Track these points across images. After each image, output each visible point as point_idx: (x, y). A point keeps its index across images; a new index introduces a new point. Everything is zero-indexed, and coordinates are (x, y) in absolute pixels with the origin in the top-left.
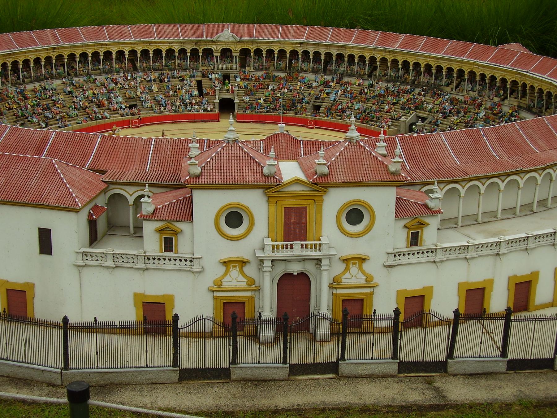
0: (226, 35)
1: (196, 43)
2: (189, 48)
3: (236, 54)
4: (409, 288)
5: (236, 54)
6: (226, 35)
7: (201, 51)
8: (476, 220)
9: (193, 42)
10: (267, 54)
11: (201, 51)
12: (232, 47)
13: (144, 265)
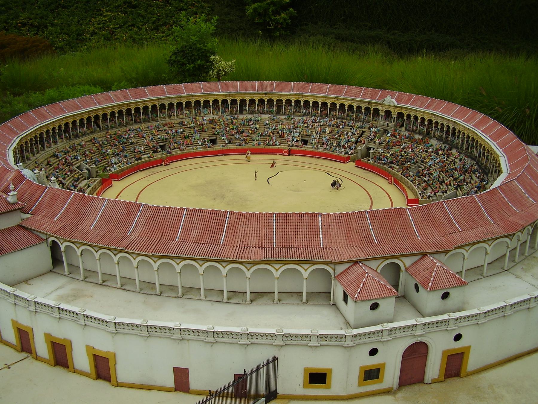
0: (390, 101)
1: (369, 103)
2: (364, 106)
3: (394, 116)
4: (118, 367)
5: (394, 116)
6: (390, 101)
7: (372, 109)
8: (502, 268)
9: (366, 102)
10: (348, 108)
11: (372, 109)
12: (392, 110)
13: (214, 339)
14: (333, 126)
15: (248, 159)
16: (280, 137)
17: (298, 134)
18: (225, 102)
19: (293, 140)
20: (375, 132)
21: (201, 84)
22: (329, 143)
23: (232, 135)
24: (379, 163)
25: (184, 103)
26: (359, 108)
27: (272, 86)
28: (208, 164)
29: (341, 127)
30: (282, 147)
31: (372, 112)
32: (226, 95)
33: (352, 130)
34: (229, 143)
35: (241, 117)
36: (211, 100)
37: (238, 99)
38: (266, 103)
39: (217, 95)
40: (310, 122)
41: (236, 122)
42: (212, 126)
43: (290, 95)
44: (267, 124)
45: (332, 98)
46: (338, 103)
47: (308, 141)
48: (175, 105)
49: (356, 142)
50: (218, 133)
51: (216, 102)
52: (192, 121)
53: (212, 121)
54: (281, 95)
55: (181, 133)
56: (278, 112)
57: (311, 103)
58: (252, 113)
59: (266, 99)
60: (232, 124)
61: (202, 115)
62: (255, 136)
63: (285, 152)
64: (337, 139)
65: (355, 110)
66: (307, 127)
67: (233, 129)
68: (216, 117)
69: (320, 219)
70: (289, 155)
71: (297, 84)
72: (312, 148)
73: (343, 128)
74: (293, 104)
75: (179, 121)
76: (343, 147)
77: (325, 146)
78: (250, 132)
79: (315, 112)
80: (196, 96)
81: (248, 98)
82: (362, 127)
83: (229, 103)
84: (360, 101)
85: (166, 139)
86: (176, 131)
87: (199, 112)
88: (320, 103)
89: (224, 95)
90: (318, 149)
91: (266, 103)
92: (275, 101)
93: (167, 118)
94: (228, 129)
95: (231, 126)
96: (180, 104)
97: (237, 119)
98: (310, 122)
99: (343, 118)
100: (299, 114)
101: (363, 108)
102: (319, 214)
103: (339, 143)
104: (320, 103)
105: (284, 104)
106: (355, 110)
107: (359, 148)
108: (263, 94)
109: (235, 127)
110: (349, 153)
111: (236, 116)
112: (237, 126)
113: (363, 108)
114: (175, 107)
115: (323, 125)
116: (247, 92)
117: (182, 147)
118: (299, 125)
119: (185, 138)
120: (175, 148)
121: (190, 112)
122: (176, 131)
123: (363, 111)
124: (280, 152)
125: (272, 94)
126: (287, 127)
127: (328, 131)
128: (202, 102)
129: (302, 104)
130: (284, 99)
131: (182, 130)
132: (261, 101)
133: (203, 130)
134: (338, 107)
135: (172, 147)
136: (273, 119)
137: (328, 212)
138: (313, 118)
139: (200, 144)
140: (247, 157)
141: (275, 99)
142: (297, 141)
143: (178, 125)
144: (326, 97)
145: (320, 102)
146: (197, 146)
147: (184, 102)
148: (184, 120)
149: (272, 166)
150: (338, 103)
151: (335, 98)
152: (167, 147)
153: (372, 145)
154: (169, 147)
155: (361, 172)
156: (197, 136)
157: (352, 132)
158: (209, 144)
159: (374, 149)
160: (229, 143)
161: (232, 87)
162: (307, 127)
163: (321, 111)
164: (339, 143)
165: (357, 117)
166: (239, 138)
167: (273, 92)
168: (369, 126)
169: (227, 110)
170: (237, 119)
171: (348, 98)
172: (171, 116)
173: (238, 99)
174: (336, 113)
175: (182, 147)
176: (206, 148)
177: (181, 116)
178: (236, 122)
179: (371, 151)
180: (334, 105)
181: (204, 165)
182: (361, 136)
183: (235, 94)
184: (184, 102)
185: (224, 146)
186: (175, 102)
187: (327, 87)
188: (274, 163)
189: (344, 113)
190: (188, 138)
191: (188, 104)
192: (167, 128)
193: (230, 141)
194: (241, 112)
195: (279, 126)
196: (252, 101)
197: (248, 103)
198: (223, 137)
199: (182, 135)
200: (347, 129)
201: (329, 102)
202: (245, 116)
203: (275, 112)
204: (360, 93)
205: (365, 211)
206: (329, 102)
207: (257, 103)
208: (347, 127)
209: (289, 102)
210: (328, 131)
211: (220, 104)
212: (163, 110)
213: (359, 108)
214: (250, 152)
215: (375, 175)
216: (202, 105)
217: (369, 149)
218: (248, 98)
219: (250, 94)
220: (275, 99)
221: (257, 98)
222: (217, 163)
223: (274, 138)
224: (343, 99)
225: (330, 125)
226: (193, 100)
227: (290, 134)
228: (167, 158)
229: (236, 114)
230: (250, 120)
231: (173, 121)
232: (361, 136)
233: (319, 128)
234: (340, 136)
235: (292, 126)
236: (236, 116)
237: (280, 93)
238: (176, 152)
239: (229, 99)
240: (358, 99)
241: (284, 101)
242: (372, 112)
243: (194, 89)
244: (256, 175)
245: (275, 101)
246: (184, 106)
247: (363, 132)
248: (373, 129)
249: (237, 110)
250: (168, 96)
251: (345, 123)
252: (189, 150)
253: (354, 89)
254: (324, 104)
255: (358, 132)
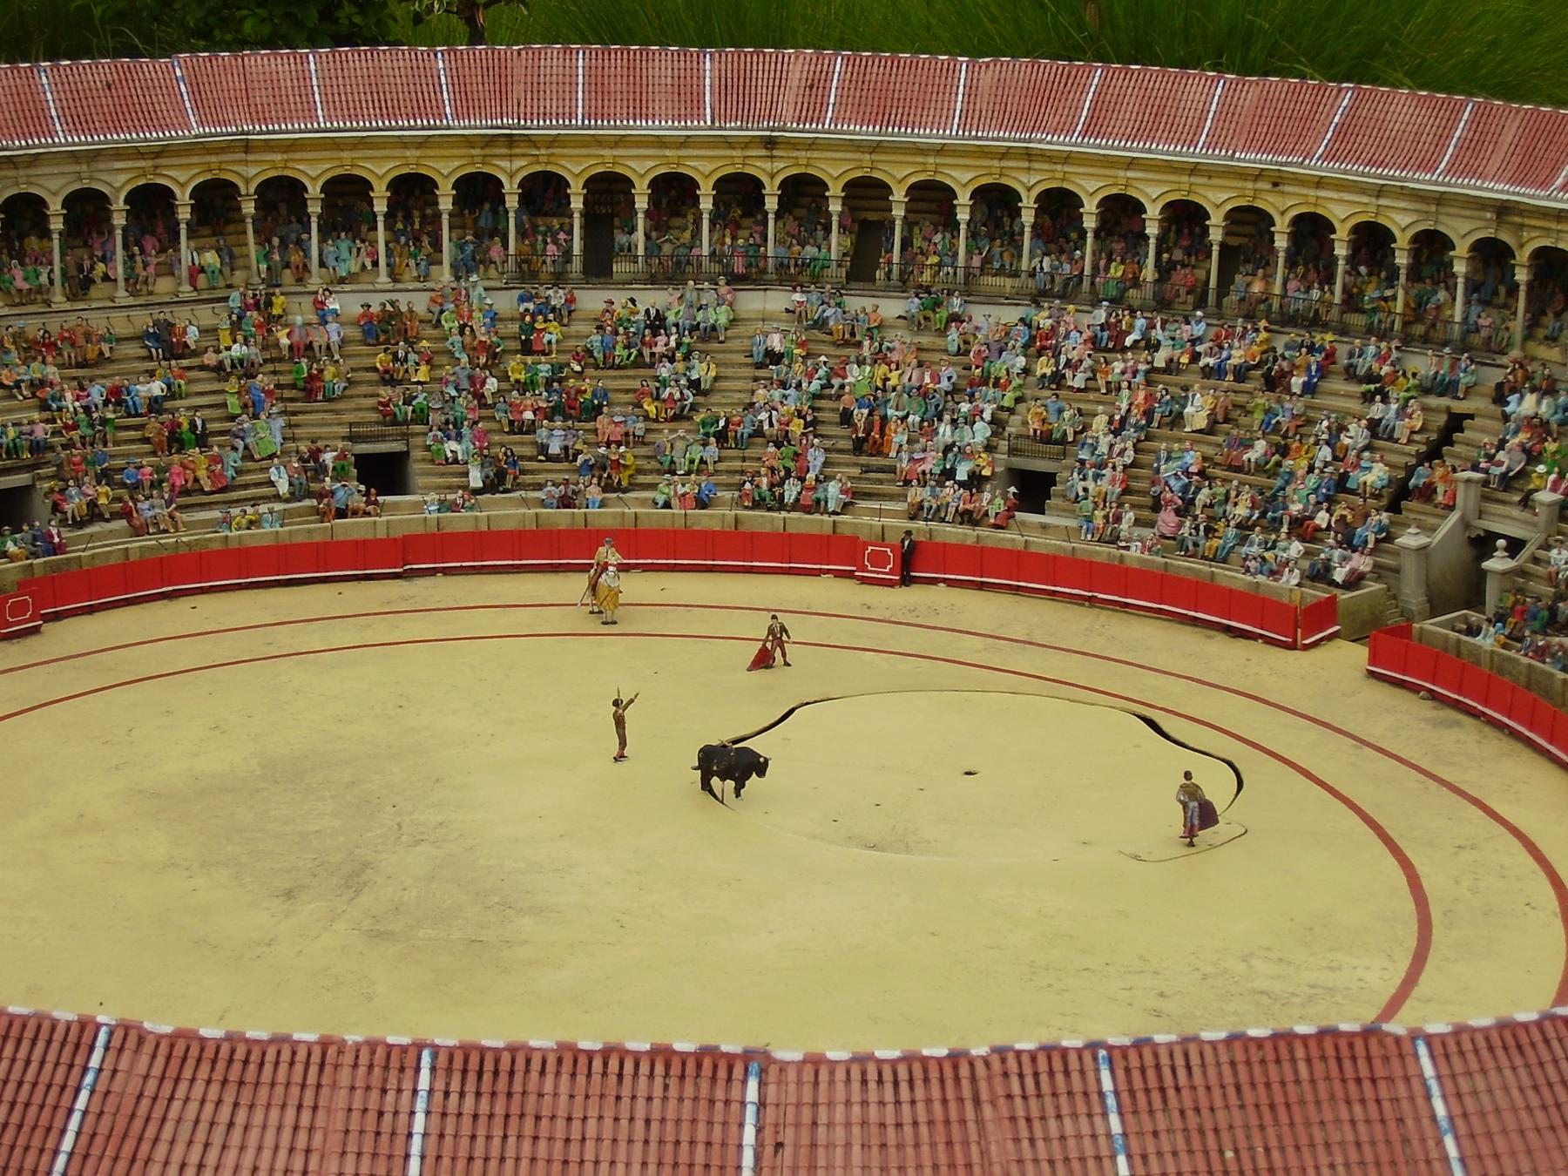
1: (1503, 210)
2: (1463, 233)
7: (1523, 256)
9: (1480, 204)
11: (1523, 256)
14: (1241, 374)
15: (604, 611)
16: (858, 447)
17: (982, 431)
18: (478, 191)
19: (949, 474)
20: (1539, 427)
21: (314, 61)
22: (1203, 496)
23: (518, 428)
24: (1541, 653)
25: (183, 197)
26: (1431, 245)
27: (815, 86)
28: (314, 638)
29: (1297, 382)
30: (866, 520)
31: (1522, 276)
32: (490, 141)
33: (1376, 410)
34: (494, 484)
35: (592, 300)
36: (380, 173)
37: (576, 171)
38: (771, 204)
39: (424, 143)
40: (1075, 347)
41: (553, 333)
42: (381, 360)
43: (941, 151)
44: (774, 357)
45: (1241, 174)
46: (1282, 210)
47: (1049, 479)
48: (119, 205)
49: (1398, 495)
50: (421, 417)
51: (412, 191)
52: (236, 326)
53: (384, 328)
54: (876, 148)
55: (155, 405)
56: (860, 271)
57: (1090, 207)
58: (670, 274)
59: (771, 173)
60: (527, 349)
61: (315, 281)
62: (681, 443)
63: (879, 560)
64: (1260, 468)
65: (1402, 259)
66: (1057, 379)
67: (523, 387)
68: (420, 303)
69: (752, 1093)
70: (907, 581)
71: (991, 71)
72: (1068, 533)
73: (1309, 389)
74: (963, 216)
75: (143, 320)
76: (1301, 528)
77: (1167, 519)
78: (650, 408)
79: (1116, 271)
80: (269, 146)
81: (641, 171)
82: (1445, 387)
83: (512, 202)
84: (1440, 200)
85: (37, 447)
86: (116, 396)
87: (295, 258)
88: (1153, 212)
89: (469, 142)
90: (1114, 539)
91: (771, 204)
92: (835, 190)
93: (58, 297)
94: (492, 384)
95: (515, 367)
96: (151, 203)
97: (564, 315)
98: (1075, 347)
99: (1314, 322)
100: (1008, 283)
101: (1462, 249)
102: (748, 1056)
103: (1269, 502)
104: (1153, 212)
105: (898, 212)
106: (1402, 259)
107: (1410, 539)
108: (747, 143)
109: (544, 370)
110: (1339, 575)
111: (557, 298)
112: (558, 368)
113: (1462, 249)
114: (119, 220)
115: (1171, 367)
116: (642, 128)
117: (147, 509)
118: (998, 368)
119: (175, 441)
120: (94, 513)
121: (231, 259)
122: (116, 396)
123: (1460, 268)
124: (838, 555)
125: (812, 145)
126: (911, 376)
127: (1197, 412)
128: (314, 190)
129: (1028, 217)
130: (899, 178)
131: (157, 388)
132: (740, 193)
133: (310, 388)
134: (1281, 242)
135: (75, 504)
136: (821, 324)
137: (816, 1047)
138: (1101, 315)
139: (283, 488)
140: (594, 587)
141: (835, 174)
142: (975, 481)
143: (133, 349)
144: (1194, 170)
145: (1153, 197)
146: (255, 501)
147: (182, 182)
148: (180, 316)
149: (763, 660)
150: (1282, 210)
151: (1259, 175)
152: (41, 506)
153: (1506, 521)
154: (56, 508)
155: (1402, 718)
156: (269, 432)
157: (1373, 425)
158: (351, 492)
159: (1515, 546)
160: (494, 484)
161: (535, 88)
162: (1057, 379)
163: (1164, 270)
164: (1269, 502)
165: (1417, 310)
166: (568, 455)
167: (829, 125)
168: (1495, 376)
169: (495, 252)
170: (564, 315)
171: (1353, 171)
172: (87, 283)
173: (576, 171)
174: (1268, 279)
175: (147, 509)
176: (323, 515)
177: (164, 285)
178: (553, 333)
179: (1498, 563)
180: (1250, 222)
181: (285, 639)
182: (1433, 454)
183: (553, 142)
184: (182, 182)
185: (453, 507)
186: (118, 184)
187: (1209, 92)
188: (778, 635)
189: (1329, 279)
190: (202, 441)
191: (215, 202)
192: (52, 372)
193: (501, 475)
194: (598, 268)
195: (854, 374)
196: (674, 192)
197: (642, 203)
198: (452, 445)
199: (153, 425)
200: (1341, 394)
201: (1217, 201)
202: (620, 298)
203: (837, 273)
204: (1441, 141)
205: (1093, 1046)
206: (1217, 201)
207: (706, 204)
208: (1337, 384)
209: (932, 199)
210: (1197, 412)
211: (446, 204)
212: (33, 242)
213: (1431, 245)
214: (614, 558)
215: (1496, 743)
216: (314, 209)
217: (1483, 544)
218: (641, 171)
219: (661, 143)
220: (835, 174)
221: (705, 171)
222: (380, 630)
223: (816, 458)
224: (1320, 183)
225: (1215, 373)
226: (249, 175)
227: (927, 428)
228: (23, 586)
229: (559, 279)
230: (657, 323)
231: (98, 322)
232: (1433, 454)
233: (1139, 390)
234: (1284, 451)
235: (948, 374)
236: (557, 298)
237: (867, 133)
238: (106, 543)
239: (510, 174)
240: (1423, 181)
241: (899, 195)
242: (1522, 276)
243: (260, 97)
244: (620, 722)
245: (835, 190)
246: (184, 214)
247: (1456, 422)
248: (1526, 405)
249: (568, 254)
250: (64, 139)
251: (1330, 356)
252: (200, 528)
253: (1402, 107)
254: (1185, 217)
255: (1411, 421)
